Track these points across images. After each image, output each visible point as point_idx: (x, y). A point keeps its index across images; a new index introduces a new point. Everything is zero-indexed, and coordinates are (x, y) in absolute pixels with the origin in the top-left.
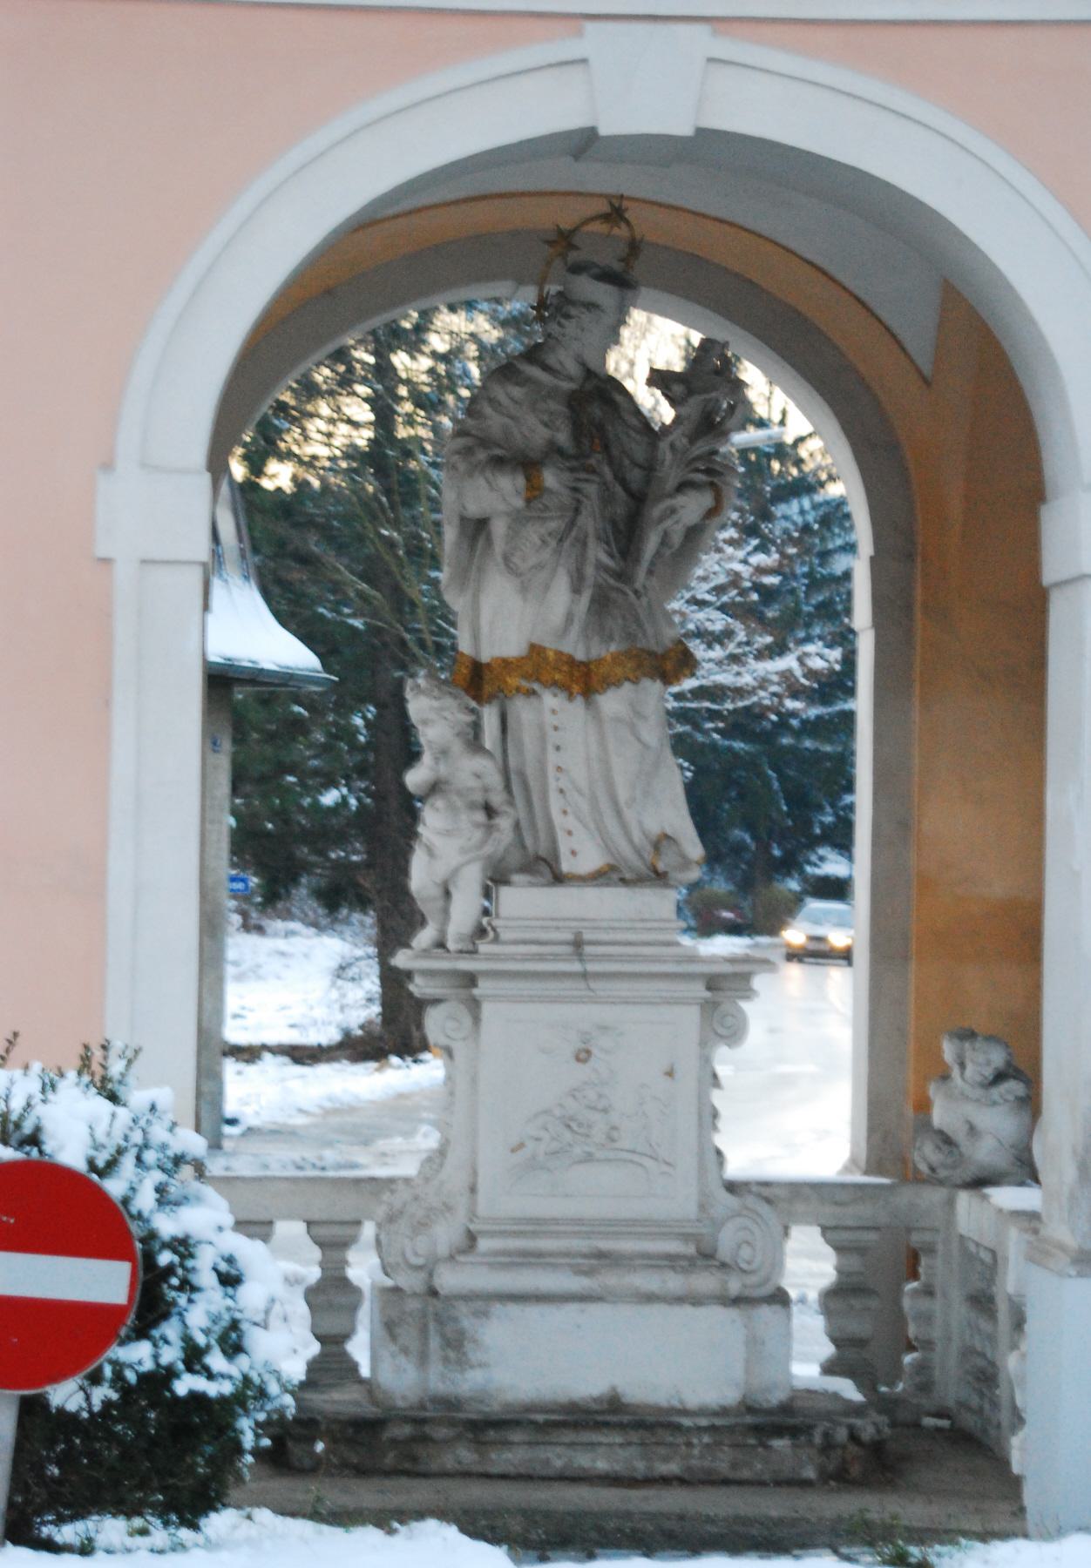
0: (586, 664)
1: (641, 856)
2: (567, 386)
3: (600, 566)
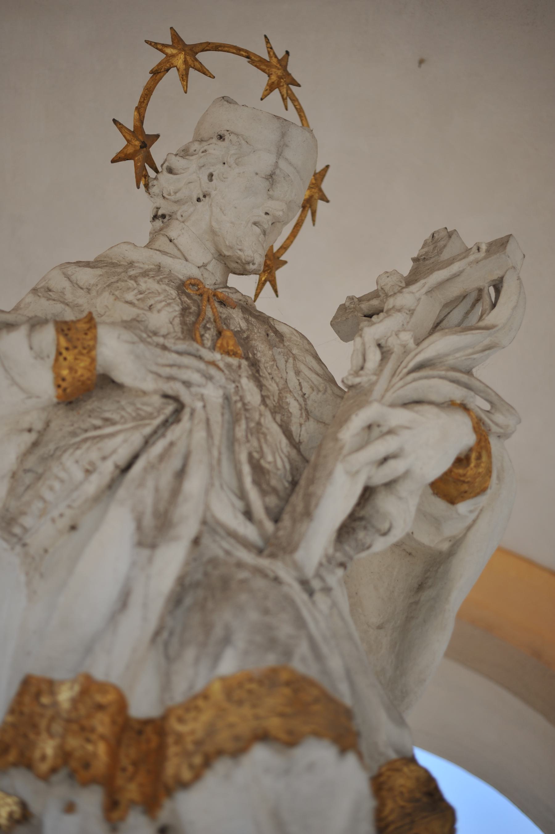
3: (209, 525)
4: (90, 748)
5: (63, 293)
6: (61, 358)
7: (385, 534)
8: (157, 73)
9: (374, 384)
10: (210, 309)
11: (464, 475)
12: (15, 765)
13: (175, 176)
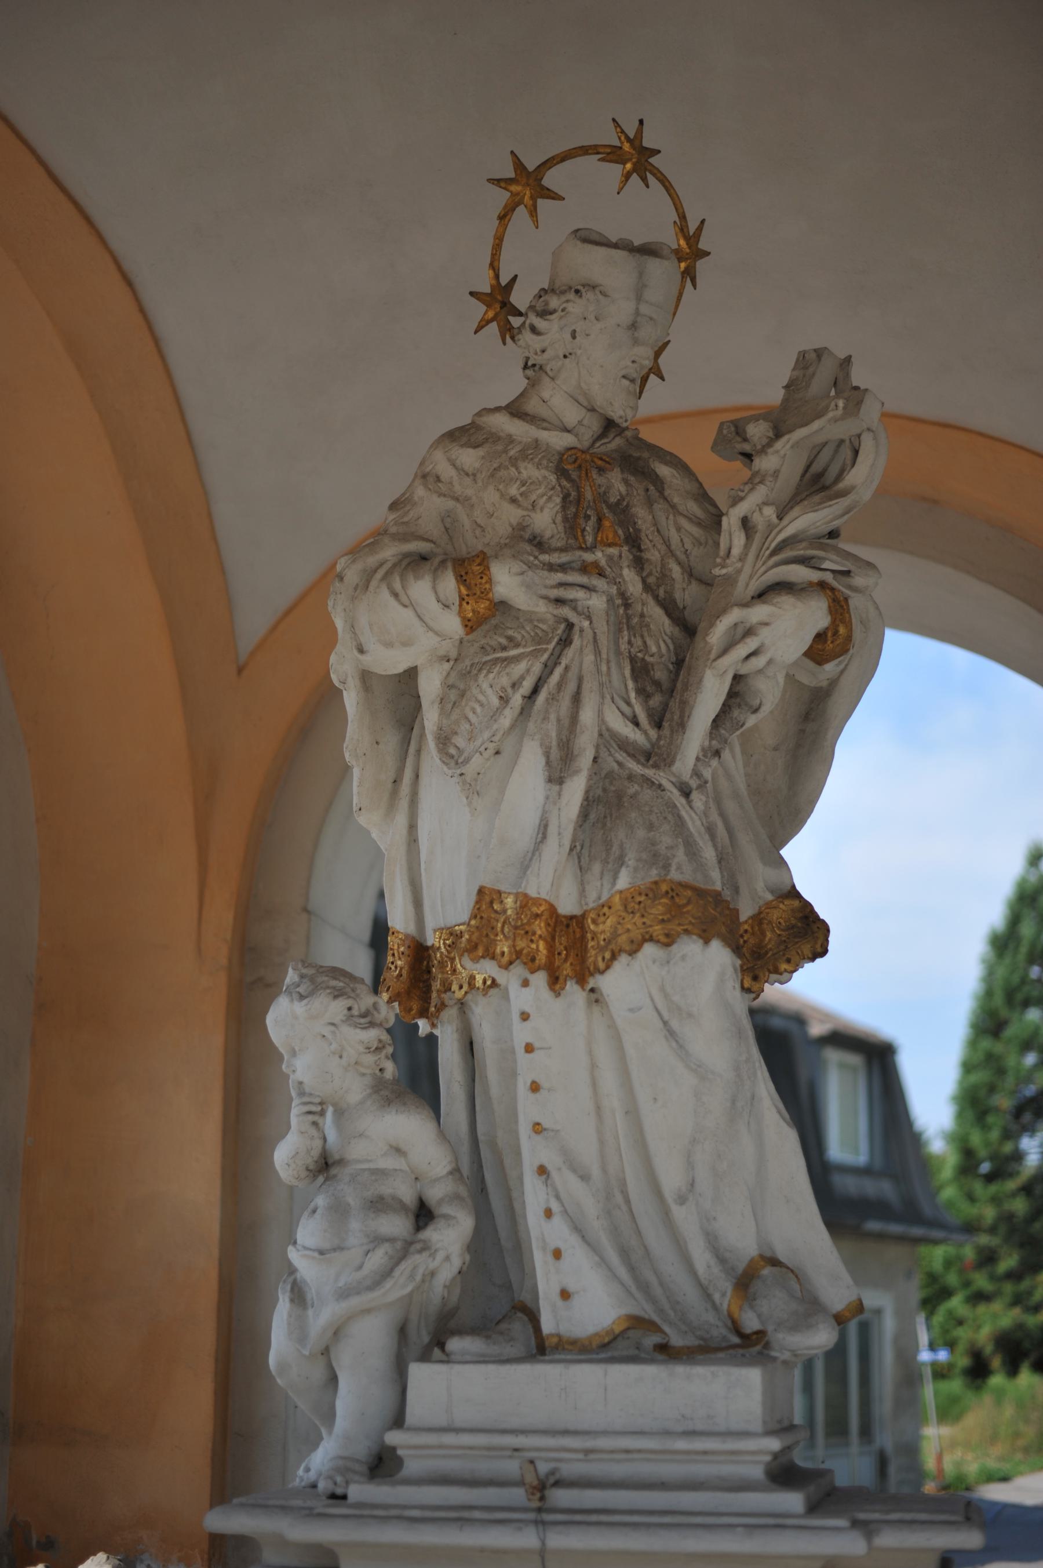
0: (577, 922)
1: (707, 1296)
2: (559, 441)
3: (607, 738)
4: (534, 946)
5: (451, 483)
6: (464, 604)
7: (756, 711)
8: (504, 217)
9: (739, 571)
10: (589, 488)
11: (823, 650)
12: (483, 957)
13: (540, 338)
